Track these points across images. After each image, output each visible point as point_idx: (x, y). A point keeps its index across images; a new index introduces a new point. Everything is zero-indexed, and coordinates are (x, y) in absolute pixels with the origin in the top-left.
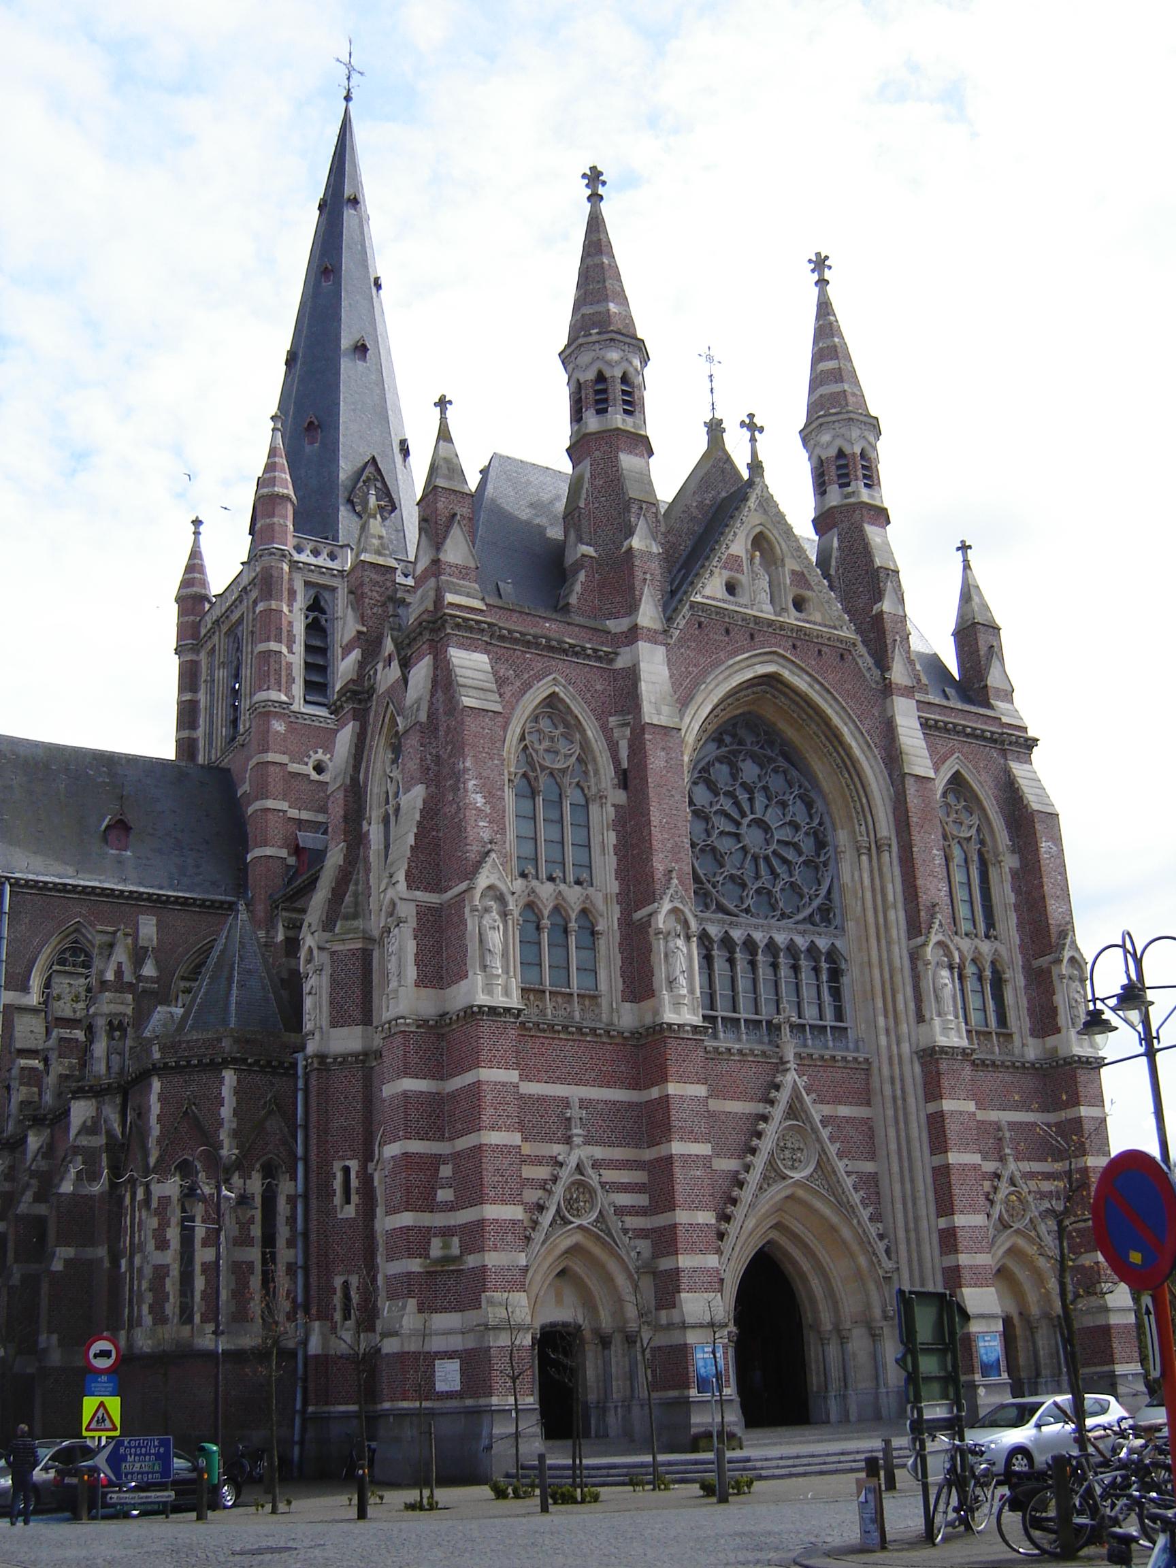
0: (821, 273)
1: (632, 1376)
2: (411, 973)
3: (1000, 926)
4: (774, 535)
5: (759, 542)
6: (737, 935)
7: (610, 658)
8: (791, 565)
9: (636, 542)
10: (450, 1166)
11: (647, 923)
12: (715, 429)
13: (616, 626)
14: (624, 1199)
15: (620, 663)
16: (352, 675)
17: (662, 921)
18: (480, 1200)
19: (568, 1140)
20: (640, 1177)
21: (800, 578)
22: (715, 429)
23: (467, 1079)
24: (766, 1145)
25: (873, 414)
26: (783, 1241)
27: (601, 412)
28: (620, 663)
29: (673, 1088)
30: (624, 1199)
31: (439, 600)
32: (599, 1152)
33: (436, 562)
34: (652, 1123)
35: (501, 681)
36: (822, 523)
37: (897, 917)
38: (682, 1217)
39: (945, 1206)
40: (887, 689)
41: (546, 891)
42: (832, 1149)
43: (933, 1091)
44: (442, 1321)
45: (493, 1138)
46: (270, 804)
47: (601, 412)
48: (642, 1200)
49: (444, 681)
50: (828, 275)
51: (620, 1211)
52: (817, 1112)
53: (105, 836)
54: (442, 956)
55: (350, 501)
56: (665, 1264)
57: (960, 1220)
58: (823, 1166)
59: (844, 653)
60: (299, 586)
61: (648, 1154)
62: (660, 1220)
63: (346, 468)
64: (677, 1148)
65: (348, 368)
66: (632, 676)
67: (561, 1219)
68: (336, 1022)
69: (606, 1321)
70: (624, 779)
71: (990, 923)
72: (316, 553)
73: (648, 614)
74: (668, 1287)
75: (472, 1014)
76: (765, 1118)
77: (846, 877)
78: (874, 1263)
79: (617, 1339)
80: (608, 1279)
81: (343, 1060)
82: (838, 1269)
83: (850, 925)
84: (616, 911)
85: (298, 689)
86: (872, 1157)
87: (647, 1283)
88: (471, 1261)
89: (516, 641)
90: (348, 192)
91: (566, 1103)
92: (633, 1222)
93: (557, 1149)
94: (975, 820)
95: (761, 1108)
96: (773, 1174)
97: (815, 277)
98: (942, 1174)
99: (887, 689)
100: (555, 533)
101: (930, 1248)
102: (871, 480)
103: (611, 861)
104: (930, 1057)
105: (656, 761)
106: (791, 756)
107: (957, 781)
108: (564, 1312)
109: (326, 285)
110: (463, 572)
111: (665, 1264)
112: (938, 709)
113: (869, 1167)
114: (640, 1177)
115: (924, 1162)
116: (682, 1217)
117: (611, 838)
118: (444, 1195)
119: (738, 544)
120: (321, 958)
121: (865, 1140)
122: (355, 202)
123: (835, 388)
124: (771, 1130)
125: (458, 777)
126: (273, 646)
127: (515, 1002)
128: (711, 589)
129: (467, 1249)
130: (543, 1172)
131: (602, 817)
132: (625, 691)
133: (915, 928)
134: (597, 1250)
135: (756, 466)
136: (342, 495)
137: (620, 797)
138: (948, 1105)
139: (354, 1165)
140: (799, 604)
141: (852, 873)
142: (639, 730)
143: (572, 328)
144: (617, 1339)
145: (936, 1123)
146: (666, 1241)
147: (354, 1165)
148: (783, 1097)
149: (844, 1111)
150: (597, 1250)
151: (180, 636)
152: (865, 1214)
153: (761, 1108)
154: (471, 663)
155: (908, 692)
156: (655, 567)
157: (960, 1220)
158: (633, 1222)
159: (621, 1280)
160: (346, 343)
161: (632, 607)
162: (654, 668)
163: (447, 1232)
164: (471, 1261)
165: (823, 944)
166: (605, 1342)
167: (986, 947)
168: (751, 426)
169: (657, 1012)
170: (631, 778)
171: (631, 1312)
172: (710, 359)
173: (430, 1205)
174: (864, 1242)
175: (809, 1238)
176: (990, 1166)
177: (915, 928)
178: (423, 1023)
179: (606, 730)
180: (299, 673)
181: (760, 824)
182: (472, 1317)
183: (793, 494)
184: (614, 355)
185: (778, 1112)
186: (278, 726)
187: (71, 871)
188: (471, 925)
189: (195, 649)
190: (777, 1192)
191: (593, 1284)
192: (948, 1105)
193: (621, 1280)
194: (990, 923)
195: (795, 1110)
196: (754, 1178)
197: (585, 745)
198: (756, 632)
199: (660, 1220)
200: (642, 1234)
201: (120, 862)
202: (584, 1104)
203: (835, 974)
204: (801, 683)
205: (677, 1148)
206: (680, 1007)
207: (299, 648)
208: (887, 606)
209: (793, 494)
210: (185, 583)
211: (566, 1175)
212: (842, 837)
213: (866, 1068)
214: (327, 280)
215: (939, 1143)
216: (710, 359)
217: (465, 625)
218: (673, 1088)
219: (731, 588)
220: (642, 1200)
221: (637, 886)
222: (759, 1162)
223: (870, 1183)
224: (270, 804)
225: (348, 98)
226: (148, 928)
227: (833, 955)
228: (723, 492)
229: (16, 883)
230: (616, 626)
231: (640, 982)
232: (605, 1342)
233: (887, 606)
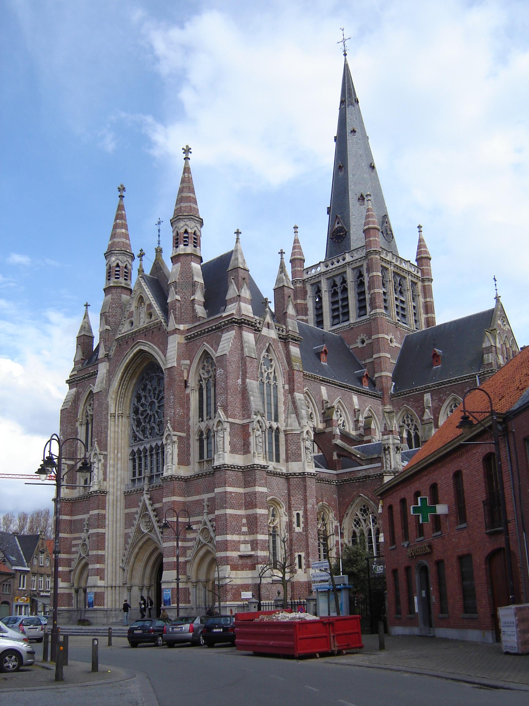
0: (187, 155)
10: (242, 531)
25: (201, 217)
50: (190, 156)
89: (214, 329)
97: (184, 156)
109: (341, 174)
112: (199, 327)
139: (303, 554)
147: (303, 554)
214: (341, 171)
225: (345, 55)
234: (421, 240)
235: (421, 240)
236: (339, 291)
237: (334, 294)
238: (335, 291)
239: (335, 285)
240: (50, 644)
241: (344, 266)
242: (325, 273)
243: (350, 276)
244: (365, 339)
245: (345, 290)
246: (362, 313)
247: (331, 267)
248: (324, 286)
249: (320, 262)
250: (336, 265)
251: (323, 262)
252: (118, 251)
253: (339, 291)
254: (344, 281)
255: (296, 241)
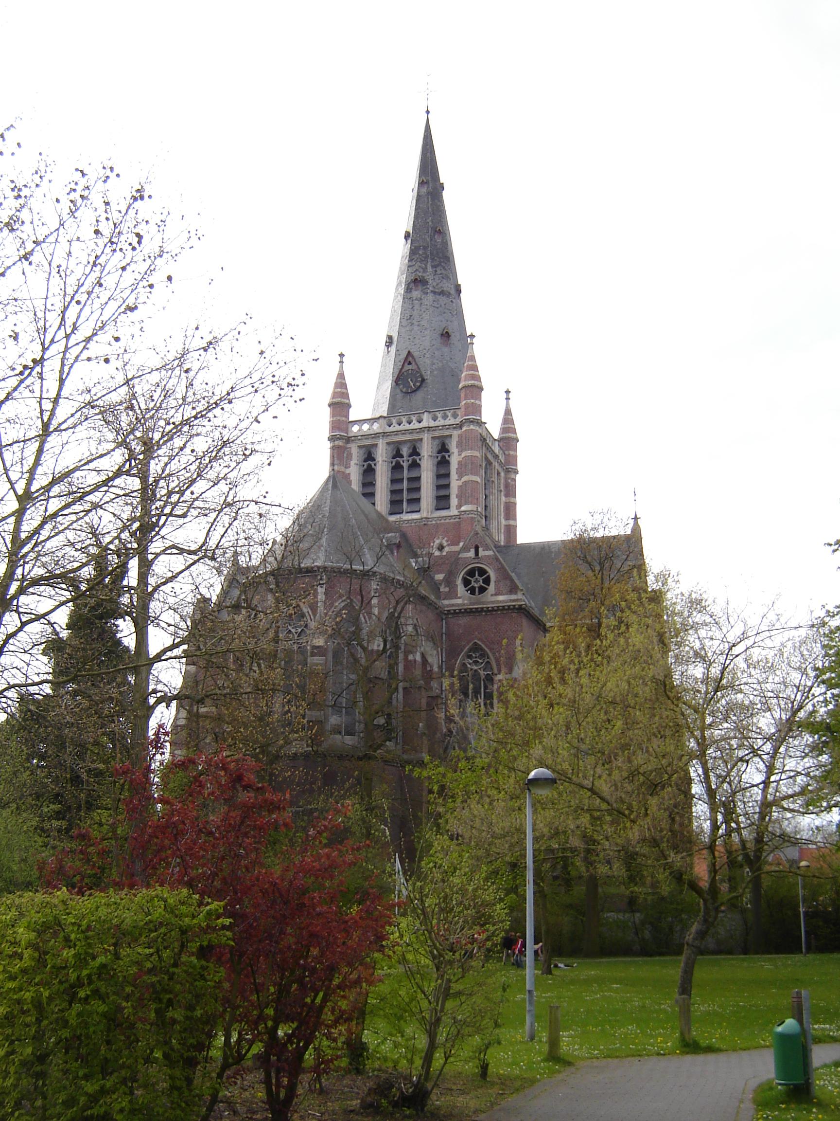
234: (341, 376)
235: (341, 376)
236: (405, 465)
237: (397, 468)
238: (398, 463)
239: (398, 454)
240: (274, 1081)
241: (422, 430)
242: (385, 434)
243: (427, 450)
244: (445, 544)
245: (415, 465)
246: (443, 503)
247: (395, 427)
248: (382, 454)
249: (381, 417)
250: (405, 426)
251: (385, 417)
252: (340, 405)
253: (405, 465)
254: (415, 452)
255: (508, 412)
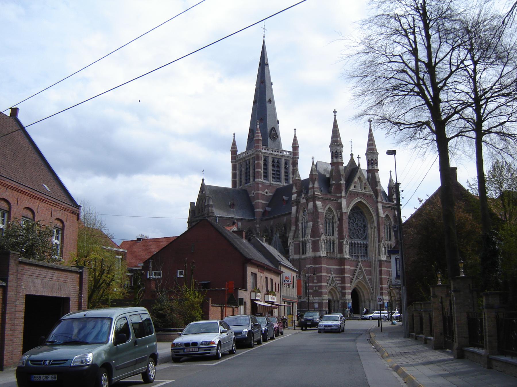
1: (338, 306)
2: (311, 250)
3: (392, 239)
4: (362, 177)
5: (359, 178)
6: (353, 242)
7: (337, 200)
8: (364, 182)
9: (342, 182)
11: (342, 242)
12: (352, 155)
13: (338, 195)
14: (338, 282)
15: (339, 201)
16: (295, 198)
17: (345, 242)
18: (321, 283)
19: (331, 274)
20: (340, 279)
21: (365, 184)
22: (352, 155)
23: (320, 266)
24: (356, 274)
26: (357, 287)
27: (336, 158)
28: (339, 201)
29: (345, 267)
30: (338, 282)
31: (314, 193)
32: (335, 275)
33: (313, 187)
34: (342, 271)
35: (323, 206)
36: (368, 171)
37: (377, 239)
38: (346, 285)
39: (381, 283)
40: (377, 202)
41: (328, 237)
42: (365, 274)
43: (380, 266)
44: (317, 298)
45: (323, 274)
46: (260, 201)
47: (336, 158)
48: (340, 282)
49: (315, 206)
51: (338, 284)
52: (363, 269)
53: (230, 206)
54: (316, 248)
55: (270, 137)
56: (343, 291)
57: (383, 286)
58: (364, 277)
59: (371, 196)
60: (262, 157)
61: (341, 276)
62: (343, 285)
63: (269, 129)
64: (346, 275)
65: (268, 105)
66: (341, 204)
67: (330, 285)
68: (295, 254)
69: (335, 298)
70: (339, 220)
71: (390, 239)
72: (265, 149)
73: (343, 194)
74: (344, 294)
75: (320, 257)
76: (356, 270)
77: (369, 232)
78: (370, 291)
79: (336, 302)
80: (335, 293)
81: (296, 260)
82: (365, 292)
83: (369, 240)
84: (337, 240)
85: (263, 177)
86: (371, 275)
87: (340, 294)
88: (320, 290)
90: (265, 62)
91: (331, 268)
92: (339, 285)
93: (330, 275)
94: (389, 222)
95: (355, 268)
96: (357, 278)
98: (381, 279)
99: (377, 202)
100: (328, 176)
101: (379, 289)
102: (377, 165)
103: (337, 232)
104: (380, 261)
105: (344, 218)
106: (362, 212)
107: (387, 216)
108: (330, 298)
110: (317, 188)
111: (343, 291)
113: (370, 277)
114: (340, 279)
115: (378, 276)
116: (346, 285)
117: (337, 229)
118: (315, 281)
119: (356, 179)
120: (292, 244)
121: (370, 273)
122: (267, 64)
123: (372, 147)
124: (357, 272)
125: (318, 222)
126: (259, 170)
127: (326, 255)
128: (352, 188)
129: (318, 289)
130: (328, 278)
131: (336, 225)
132: (339, 206)
133: (379, 241)
134: (334, 289)
135: (359, 165)
136: (268, 135)
137: (338, 222)
138: (383, 269)
140: (365, 188)
141: (370, 231)
142: (342, 213)
143: (331, 141)
144: (336, 302)
145: (381, 271)
146: (344, 288)
148: (359, 267)
149: (367, 269)
150: (334, 289)
151: (232, 159)
152: (369, 284)
153: (355, 268)
154: (319, 203)
155: (381, 202)
156: (344, 185)
157: (383, 286)
158: (339, 285)
159: (337, 293)
160: (267, 100)
161: (341, 193)
162: (344, 202)
163: (316, 286)
164: (320, 290)
165: (365, 243)
166: (334, 302)
167: (389, 243)
168: (359, 158)
169: (343, 256)
170: (340, 220)
171: (339, 297)
172: (351, 142)
173: (314, 283)
174: (369, 288)
175: (361, 287)
176: (388, 277)
177: (379, 241)
178: (313, 257)
179: (336, 212)
180: (263, 174)
181: (357, 224)
182: (320, 298)
183: (364, 166)
184: (339, 148)
185: (358, 269)
186: (260, 186)
187: (226, 214)
188: (320, 244)
189: (236, 162)
190: (358, 280)
191: (334, 295)
192: (383, 269)
193: (337, 293)
194: (390, 239)
195: (360, 269)
196: (354, 279)
197: (333, 214)
198: (358, 194)
199: (343, 285)
200: (340, 287)
201: (234, 212)
202: (333, 268)
203: (367, 247)
204: (364, 202)
205: (346, 275)
206: (347, 256)
207: (263, 169)
208: (378, 188)
209: (364, 166)
210: (232, 148)
211: (331, 279)
212: (369, 226)
213: (370, 262)
215: (381, 274)
216: (351, 142)
217: (318, 198)
218: (345, 267)
219: (355, 187)
220: (340, 282)
221: (341, 237)
222: (355, 276)
223: (370, 279)
224: (260, 201)
225: (264, 37)
226: (240, 224)
227: (366, 244)
228: (353, 168)
229: (219, 217)
230: (338, 195)
231: (341, 251)
232: (334, 302)
233: (378, 188)
